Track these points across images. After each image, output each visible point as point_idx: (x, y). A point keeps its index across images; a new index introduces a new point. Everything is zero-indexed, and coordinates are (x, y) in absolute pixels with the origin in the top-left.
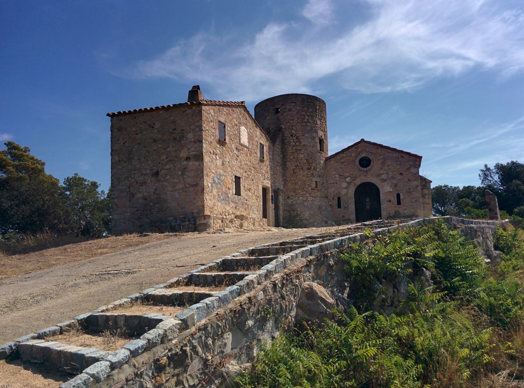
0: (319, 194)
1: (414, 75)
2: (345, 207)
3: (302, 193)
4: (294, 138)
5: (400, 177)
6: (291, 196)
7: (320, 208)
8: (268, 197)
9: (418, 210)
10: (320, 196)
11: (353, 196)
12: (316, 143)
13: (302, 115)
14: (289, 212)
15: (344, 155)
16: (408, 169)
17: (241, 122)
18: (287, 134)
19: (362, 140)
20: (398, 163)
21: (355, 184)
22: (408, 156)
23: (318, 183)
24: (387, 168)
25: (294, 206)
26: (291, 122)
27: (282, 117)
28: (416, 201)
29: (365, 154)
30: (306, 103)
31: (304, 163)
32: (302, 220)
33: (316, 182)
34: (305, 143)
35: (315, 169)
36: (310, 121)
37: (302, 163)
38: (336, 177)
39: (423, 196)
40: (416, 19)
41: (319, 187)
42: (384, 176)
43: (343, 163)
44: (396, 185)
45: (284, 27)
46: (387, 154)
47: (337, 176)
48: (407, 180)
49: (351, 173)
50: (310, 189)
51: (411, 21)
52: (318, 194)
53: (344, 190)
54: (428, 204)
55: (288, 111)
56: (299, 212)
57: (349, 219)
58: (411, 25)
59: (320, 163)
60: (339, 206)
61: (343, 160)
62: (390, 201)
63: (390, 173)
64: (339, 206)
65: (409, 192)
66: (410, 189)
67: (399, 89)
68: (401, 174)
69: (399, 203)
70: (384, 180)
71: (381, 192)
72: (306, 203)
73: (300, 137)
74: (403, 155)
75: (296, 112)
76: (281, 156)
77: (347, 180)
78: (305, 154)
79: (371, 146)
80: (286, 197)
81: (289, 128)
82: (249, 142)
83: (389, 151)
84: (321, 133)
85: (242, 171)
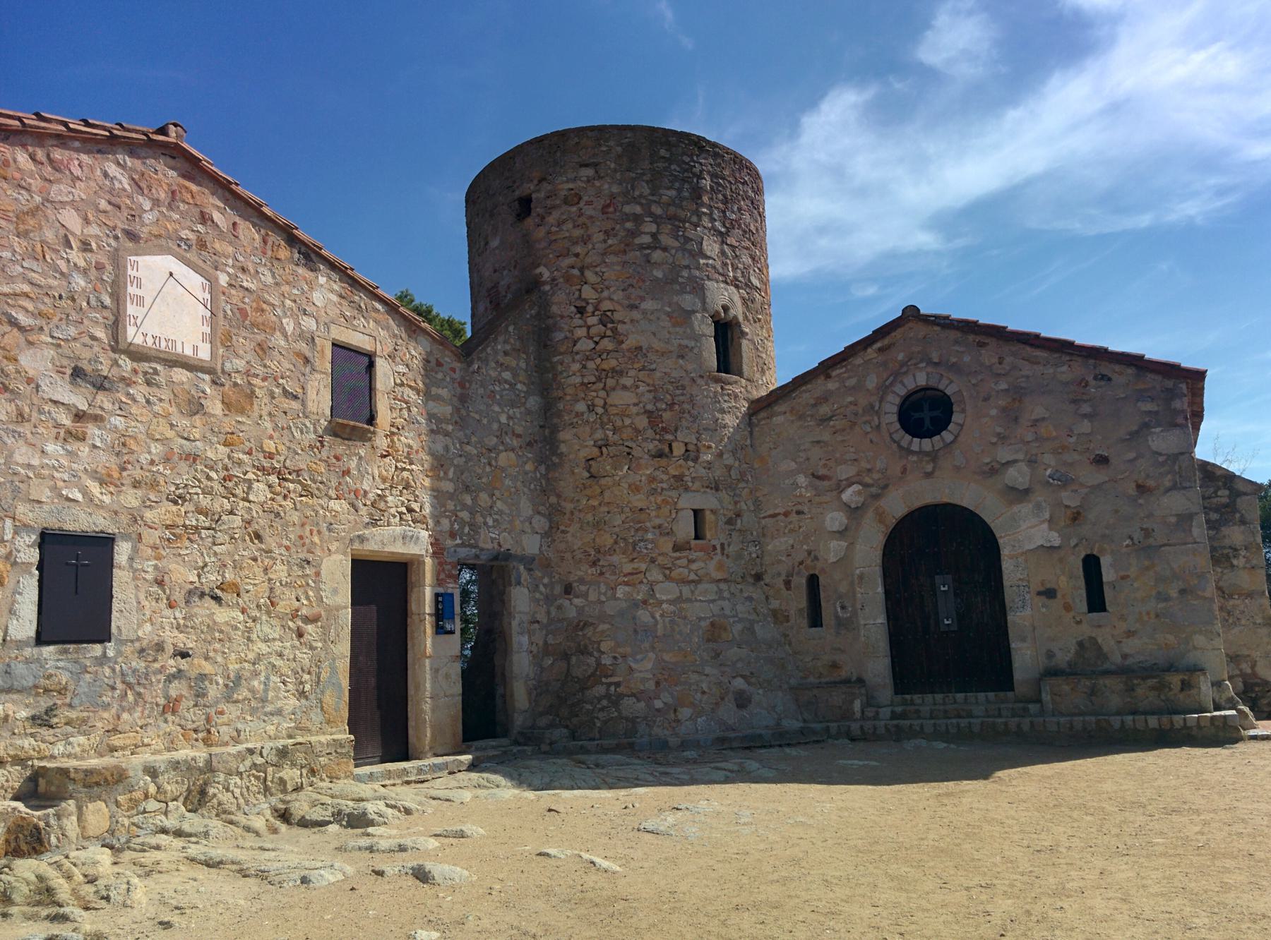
0: (712, 565)
1: (1213, 181)
2: (841, 624)
3: (628, 568)
4: (592, 320)
5: (1096, 476)
6: (581, 581)
7: (715, 631)
8: (413, 606)
9: (1199, 640)
10: (719, 576)
11: (877, 571)
12: (697, 338)
13: (627, 217)
14: (566, 657)
15: (832, 385)
16: (1134, 435)
17: (144, 232)
18: (560, 304)
19: (911, 313)
20: (1086, 408)
21: (880, 516)
22: (1130, 371)
23: (709, 517)
24: (1030, 437)
25: (589, 632)
26: (578, 249)
27: (541, 233)
28: (1183, 592)
29: (927, 372)
30: (646, 165)
31: (638, 431)
32: (615, 701)
33: (697, 513)
34: (643, 341)
35: (691, 454)
36: (666, 240)
37: (627, 433)
38: (797, 486)
39: (1221, 557)
40: (1215, 40)
41: (713, 535)
42: (1017, 476)
43: (824, 420)
44: (1076, 517)
45: (870, 93)
46: (1027, 369)
47: (801, 480)
48: (1132, 490)
49: (865, 465)
50: (666, 545)
51: (1201, 47)
52: (711, 567)
53: (834, 544)
54: (1250, 595)
55: (566, 201)
56: (606, 661)
57: (861, 681)
58: (1199, 57)
59: (717, 427)
60: (815, 619)
61: (824, 410)
62: (1050, 593)
63: (1048, 459)
64: (815, 619)
65: (1146, 548)
66: (1147, 533)
67: (1172, 217)
68: (1102, 461)
69: (1096, 601)
70: (1018, 494)
71: (1005, 552)
72: (643, 615)
73: (617, 316)
74: (1106, 368)
75: (599, 203)
76: (533, 402)
77: (847, 496)
78: (643, 388)
79: (953, 335)
80: (558, 589)
81: (568, 279)
82: (221, 339)
83: (1039, 353)
84: (722, 295)
85: (131, 498)
